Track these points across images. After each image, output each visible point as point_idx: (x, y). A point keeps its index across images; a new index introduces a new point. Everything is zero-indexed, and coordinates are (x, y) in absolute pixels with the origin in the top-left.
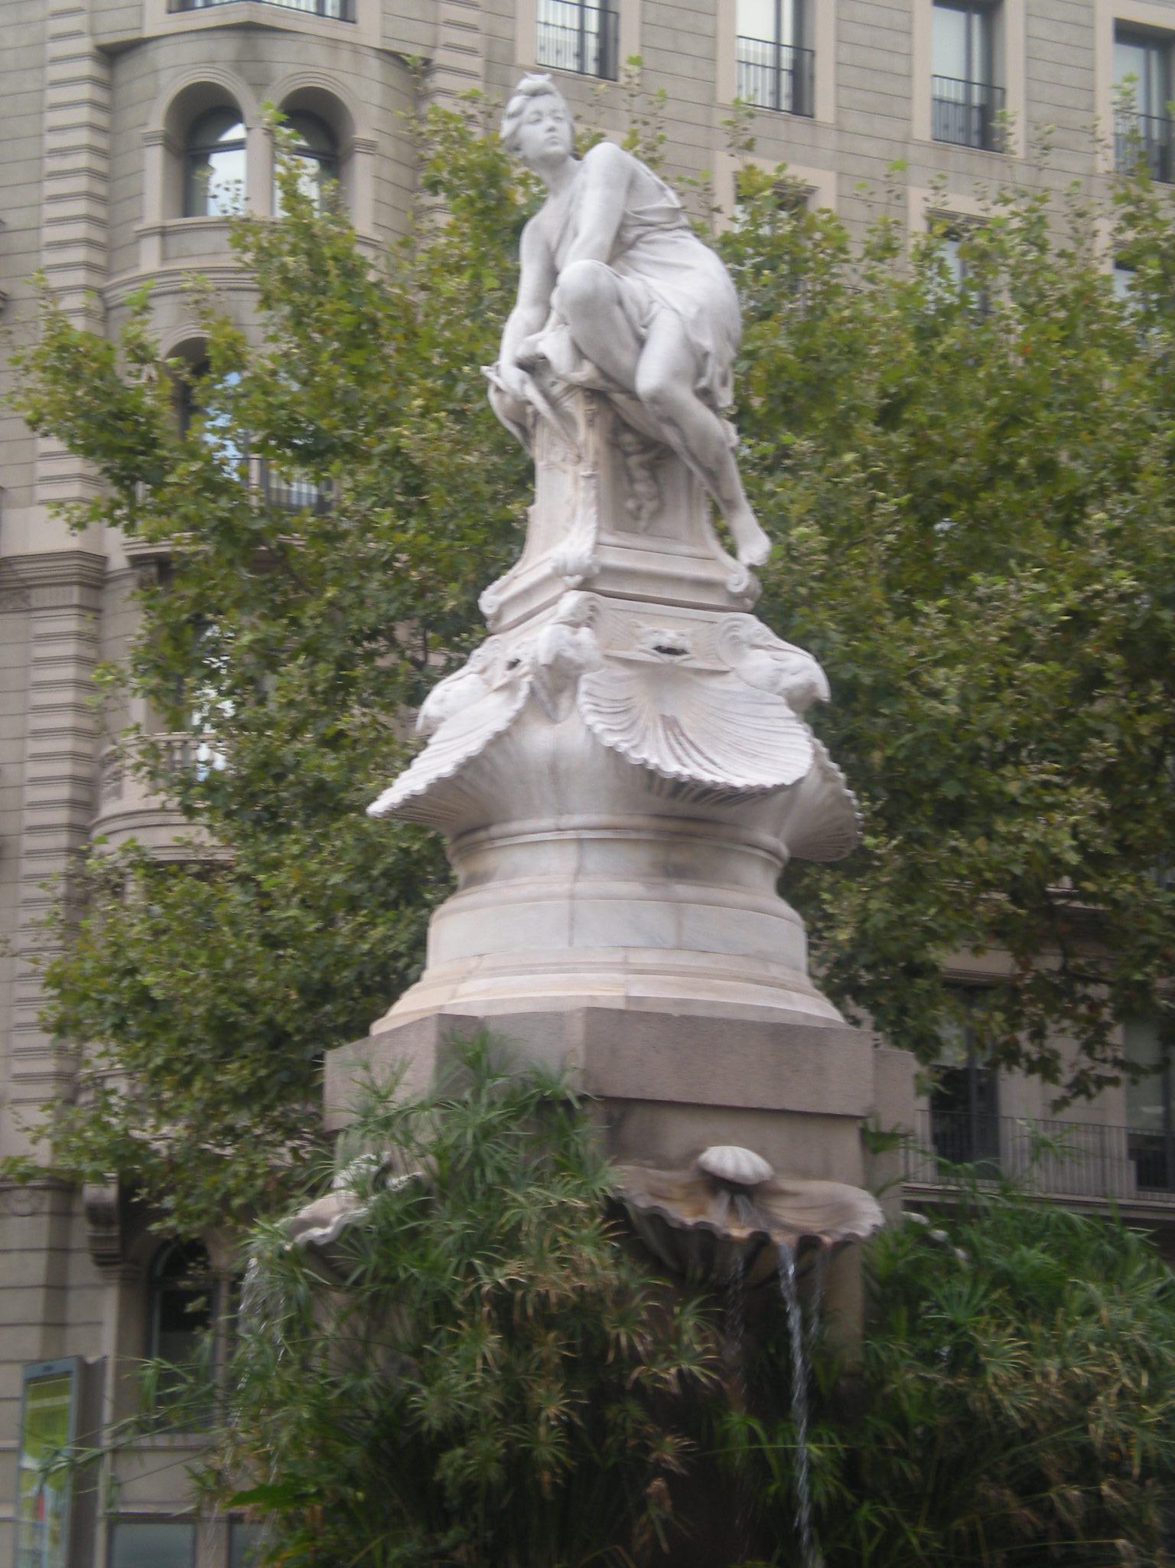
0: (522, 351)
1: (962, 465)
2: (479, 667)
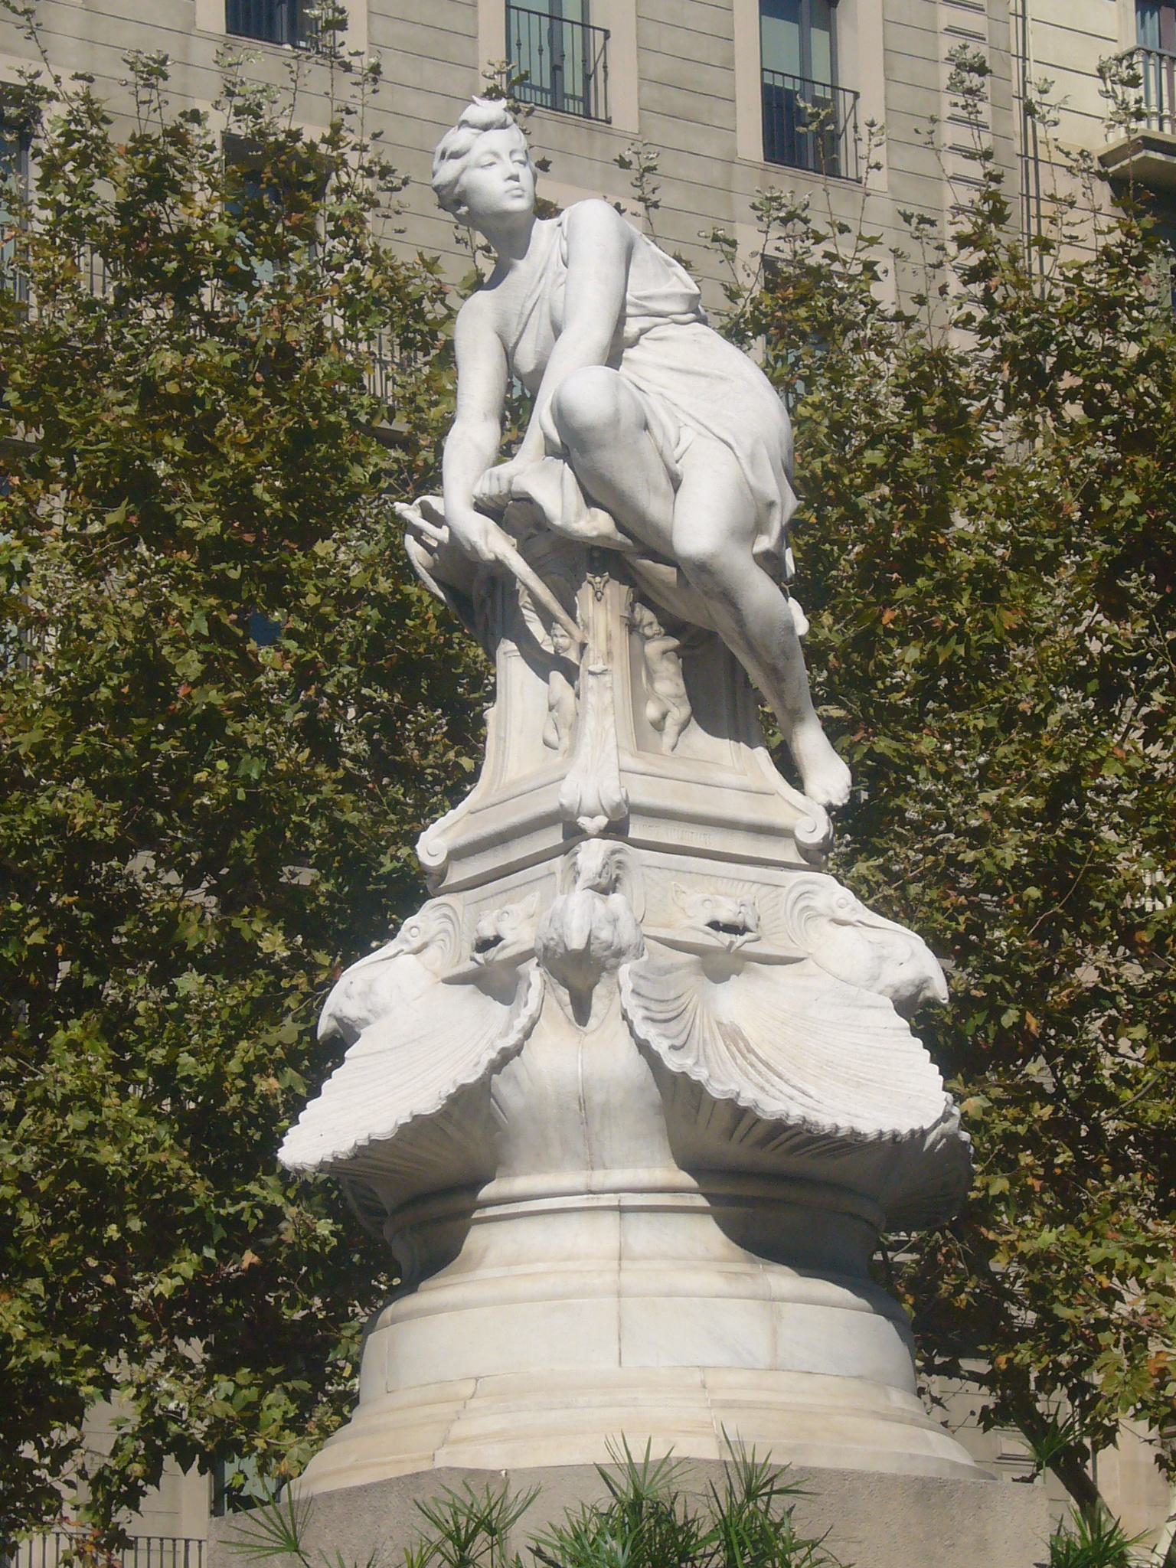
0: (486, 487)
1: (1157, 825)
2: (416, 943)
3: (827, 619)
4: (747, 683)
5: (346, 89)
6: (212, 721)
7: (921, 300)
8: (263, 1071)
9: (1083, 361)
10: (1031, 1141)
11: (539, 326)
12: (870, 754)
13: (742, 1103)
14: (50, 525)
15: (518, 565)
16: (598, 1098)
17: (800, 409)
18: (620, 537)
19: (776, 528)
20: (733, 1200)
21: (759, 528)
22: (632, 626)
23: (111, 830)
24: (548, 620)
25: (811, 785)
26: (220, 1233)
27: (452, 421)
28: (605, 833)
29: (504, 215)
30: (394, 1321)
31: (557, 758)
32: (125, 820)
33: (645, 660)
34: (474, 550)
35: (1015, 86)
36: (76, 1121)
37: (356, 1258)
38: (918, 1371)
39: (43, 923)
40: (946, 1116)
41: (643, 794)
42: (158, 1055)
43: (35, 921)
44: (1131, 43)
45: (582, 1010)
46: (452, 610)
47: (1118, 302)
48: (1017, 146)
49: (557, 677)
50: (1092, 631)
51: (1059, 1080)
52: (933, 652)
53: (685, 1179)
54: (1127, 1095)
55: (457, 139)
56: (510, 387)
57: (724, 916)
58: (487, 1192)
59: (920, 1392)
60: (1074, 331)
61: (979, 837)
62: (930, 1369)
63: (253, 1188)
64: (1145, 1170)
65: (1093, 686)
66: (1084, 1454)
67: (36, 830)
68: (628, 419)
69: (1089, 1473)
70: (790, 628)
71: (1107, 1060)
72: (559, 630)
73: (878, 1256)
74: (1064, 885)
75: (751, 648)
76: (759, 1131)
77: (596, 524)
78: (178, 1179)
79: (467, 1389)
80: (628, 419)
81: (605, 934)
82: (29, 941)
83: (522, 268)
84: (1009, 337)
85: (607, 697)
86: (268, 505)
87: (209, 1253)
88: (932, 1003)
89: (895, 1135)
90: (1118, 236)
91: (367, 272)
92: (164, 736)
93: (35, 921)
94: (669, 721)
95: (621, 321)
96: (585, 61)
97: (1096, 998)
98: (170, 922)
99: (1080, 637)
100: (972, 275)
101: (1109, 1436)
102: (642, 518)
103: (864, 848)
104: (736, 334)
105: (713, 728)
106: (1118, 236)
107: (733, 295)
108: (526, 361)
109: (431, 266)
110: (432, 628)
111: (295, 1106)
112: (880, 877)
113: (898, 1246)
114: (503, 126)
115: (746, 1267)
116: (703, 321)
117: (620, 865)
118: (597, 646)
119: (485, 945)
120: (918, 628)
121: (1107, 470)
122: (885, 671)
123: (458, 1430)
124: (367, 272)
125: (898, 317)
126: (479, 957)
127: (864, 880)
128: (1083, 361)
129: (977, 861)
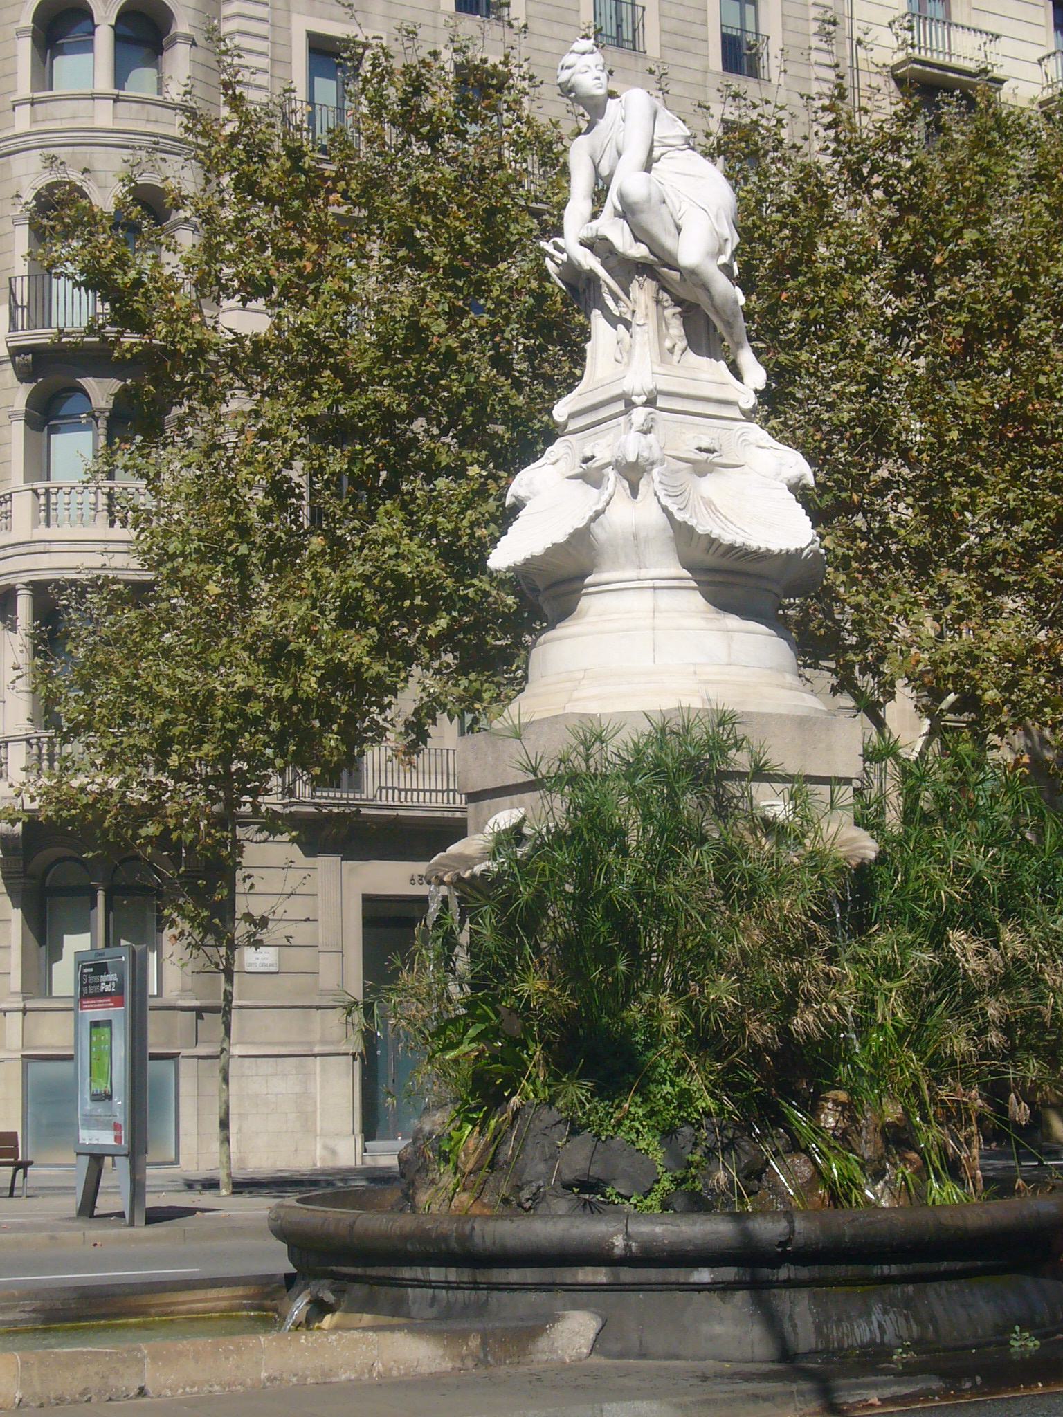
0: (586, 233)
2: (553, 460)
3: (754, 297)
4: (715, 329)
5: (510, 37)
6: (450, 354)
7: (806, 138)
8: (479, 525)
9: (884, 168)
10: (857, 558)
11: (611, 153)
12: (777, 364)
13: (713, 536)
14: (372, 257)
15: (602, 272)
16: (642, 534)
17: (741, 193)
18: (652, 257)
19: (729, 252)
20: (709, 583)
21: (721, 252)
22: (658, 302)
23: (404, 407)
24: (616, 299)
25: (745, 380)
26: (459, 604)
27: (566, 203)
28: (645, 404)
29: (593, 97)
30: (545, 643)
31: (621, 368)
32: (410, 403)
33: (665, 318)
34: (580, 264)
35: (847, 33)
36: (389, 550)
37: (526, 615)
38: (800, 666)
39: (373, 453)
40: (813, 542)
41: (663, 386)
42: (428, 518)
43: (368, 452)
44: (905, 10)
45: (634, 492)
46: (569, 295)
47: (901, 139)
48: (848, 63)
49: (621, 327)
50: (888, 304)
51: (869, 524)
52: (807, 313)
53: (686, 573)
54: (902, 532)
55: (569, 59)
56: (597, 184)
57: (704, 445)
58: (588, 580)
59: (800, 676)
60: (880, 154)
61: (831, 406)
62: (805, 665)
63: (475, 582)
64: (911, 568)
65: (888, 330)
66: (882, 706)
67: (367, 407)
68: (655, 198)
69: (881, 713)
70: (736, 302)
71: (892, 515)
72: (621, 304)
73: (781, 612)
74: (874, 427)
75: (717, 312)
76: (721, 550)
77: (639, 251)
78: (439, 578)
79: (581, 675)
80: (655, 198)
81: (646, 454)
82: (367, 462)
83: (602, 124)
84: (849, 157)
85: (646, 336)
86: (472, 246)
87: (455, 614)
88: (805, 487)
89: (788, 551)
90: (901, 106)
91: (524, 129)
92: (429, 362)
93: (368, 452)
94: (676, 348)
95: (651, 149)
96: (633, 22)
97: (887, 484)
98: (432, 455)
99: (881, 307)
100: (828, 127)
101: (891, 696)
102: (663, 248)
103: (775, 413)
104: (709, 155)
105: (697, 351)
106: (901, 106)
107: (708, 135)
108: (604, 171)
109: (556, 125)
110: (559, 306)
111: (494, 541)
112: (781, 427)
113: (790, 606)
114: (592, 52)
115: (715, 616)
116: (693, 149)
117: (653, 420)
118: (640, 312)
119: (586, 460)
120: (800, 301)
121: (894, 222)
122: (784, 324)
123: (576, 695)
124: (524, 129)
125: (794, 146)
126: (584, 466)
127: (773, 428)
128: (884, 168)
129: (830, 418)
